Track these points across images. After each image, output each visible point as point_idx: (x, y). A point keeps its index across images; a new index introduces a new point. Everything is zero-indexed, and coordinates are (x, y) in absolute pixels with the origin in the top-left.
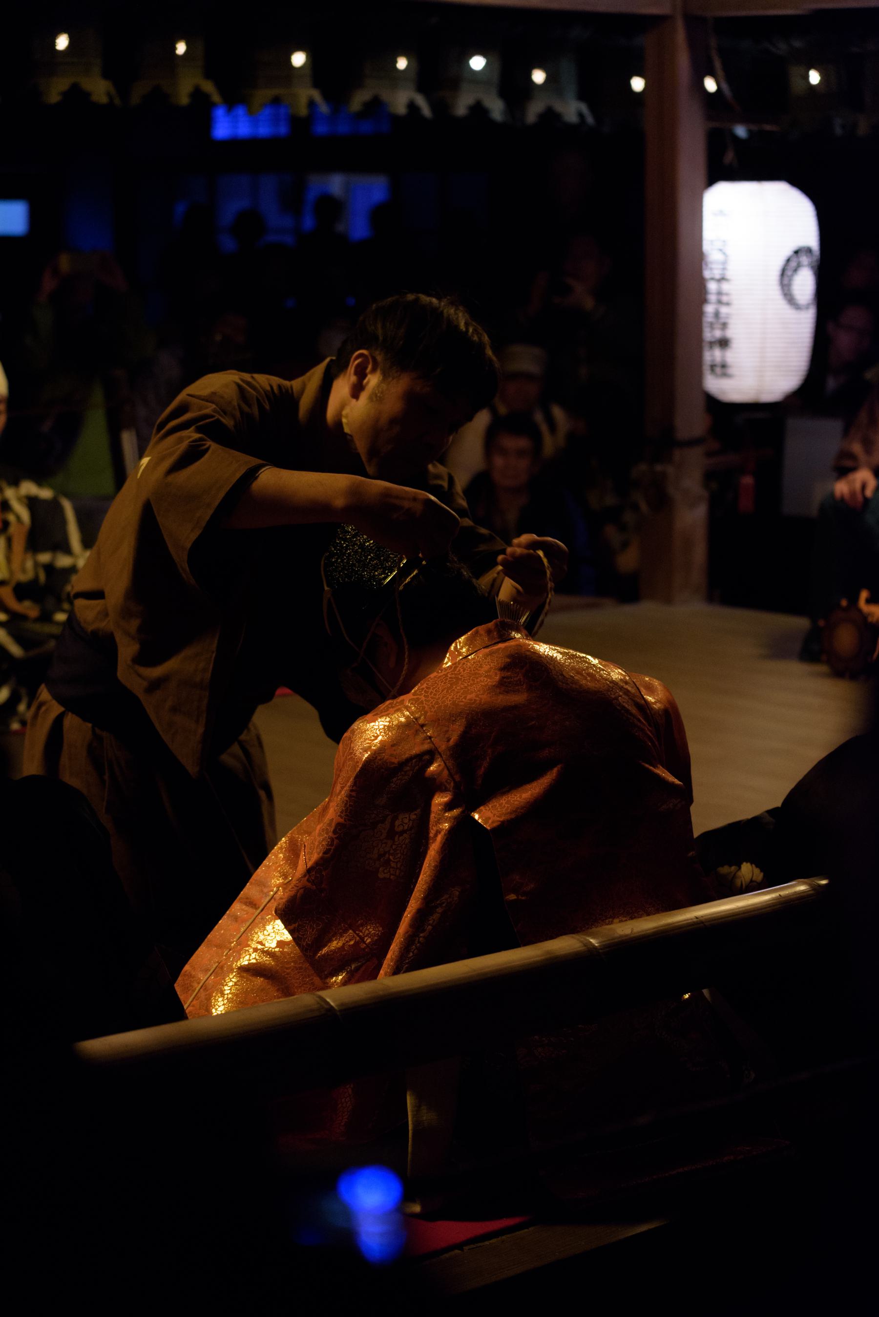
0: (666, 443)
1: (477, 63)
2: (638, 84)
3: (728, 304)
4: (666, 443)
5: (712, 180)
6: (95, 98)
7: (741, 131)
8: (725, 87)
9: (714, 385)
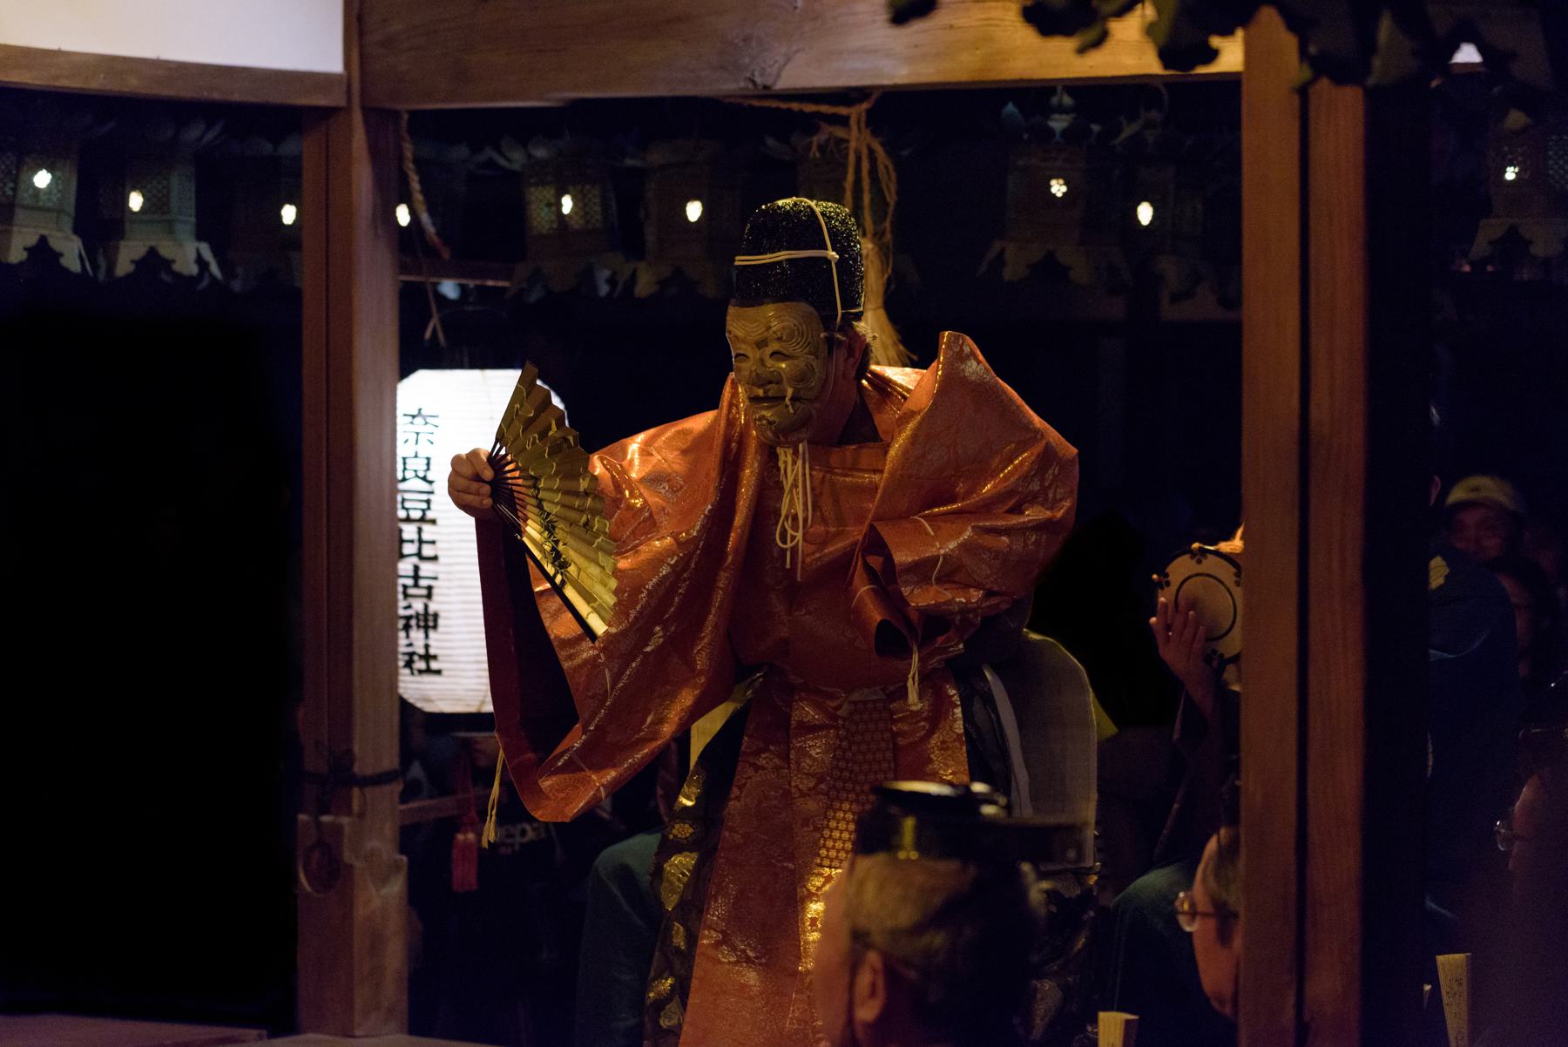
0: (341, 779)
1: (42, 179)
2: (289, 214)
3: (433, 522)
4: (341, 779)
5: (405, 373)
6: (64, 262)
7: (449, 289)
8: (425, 218)
9: (412, 687)
